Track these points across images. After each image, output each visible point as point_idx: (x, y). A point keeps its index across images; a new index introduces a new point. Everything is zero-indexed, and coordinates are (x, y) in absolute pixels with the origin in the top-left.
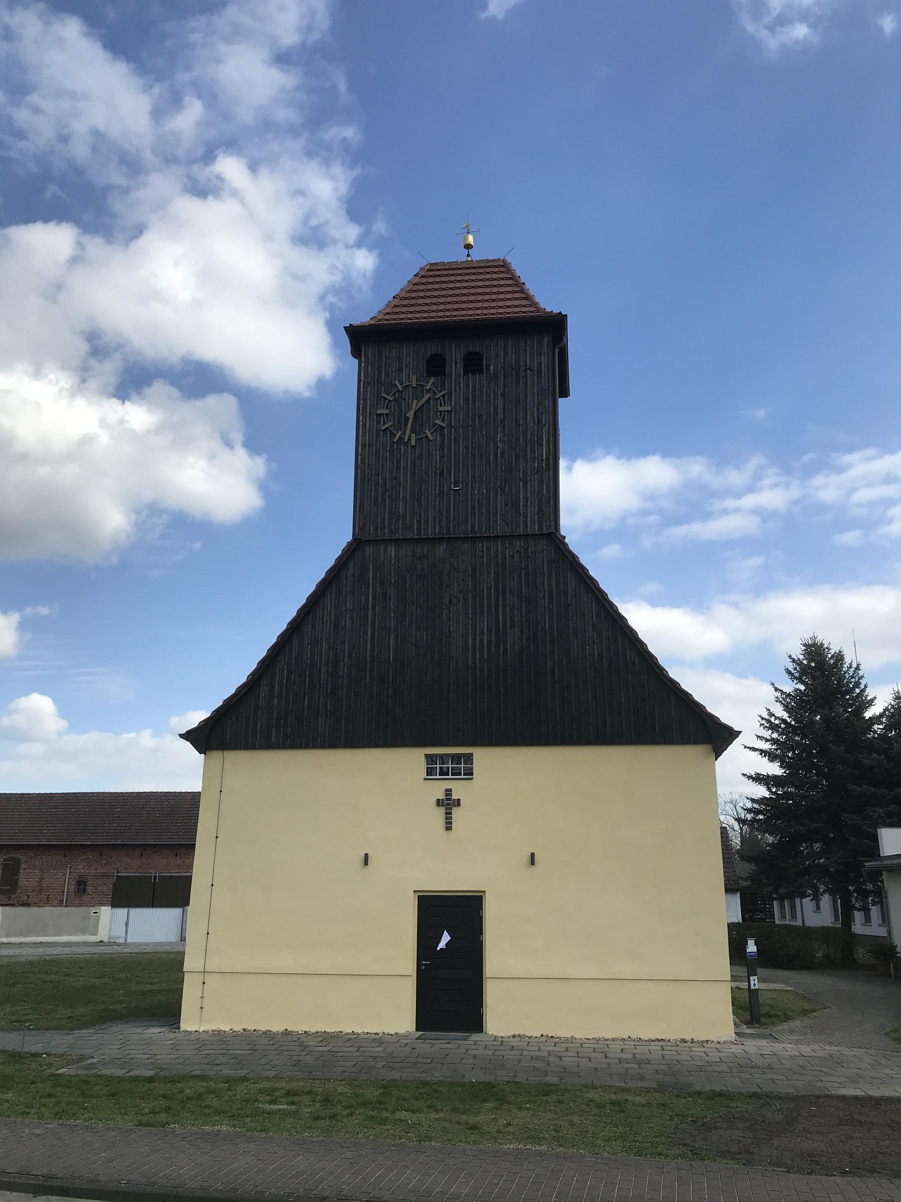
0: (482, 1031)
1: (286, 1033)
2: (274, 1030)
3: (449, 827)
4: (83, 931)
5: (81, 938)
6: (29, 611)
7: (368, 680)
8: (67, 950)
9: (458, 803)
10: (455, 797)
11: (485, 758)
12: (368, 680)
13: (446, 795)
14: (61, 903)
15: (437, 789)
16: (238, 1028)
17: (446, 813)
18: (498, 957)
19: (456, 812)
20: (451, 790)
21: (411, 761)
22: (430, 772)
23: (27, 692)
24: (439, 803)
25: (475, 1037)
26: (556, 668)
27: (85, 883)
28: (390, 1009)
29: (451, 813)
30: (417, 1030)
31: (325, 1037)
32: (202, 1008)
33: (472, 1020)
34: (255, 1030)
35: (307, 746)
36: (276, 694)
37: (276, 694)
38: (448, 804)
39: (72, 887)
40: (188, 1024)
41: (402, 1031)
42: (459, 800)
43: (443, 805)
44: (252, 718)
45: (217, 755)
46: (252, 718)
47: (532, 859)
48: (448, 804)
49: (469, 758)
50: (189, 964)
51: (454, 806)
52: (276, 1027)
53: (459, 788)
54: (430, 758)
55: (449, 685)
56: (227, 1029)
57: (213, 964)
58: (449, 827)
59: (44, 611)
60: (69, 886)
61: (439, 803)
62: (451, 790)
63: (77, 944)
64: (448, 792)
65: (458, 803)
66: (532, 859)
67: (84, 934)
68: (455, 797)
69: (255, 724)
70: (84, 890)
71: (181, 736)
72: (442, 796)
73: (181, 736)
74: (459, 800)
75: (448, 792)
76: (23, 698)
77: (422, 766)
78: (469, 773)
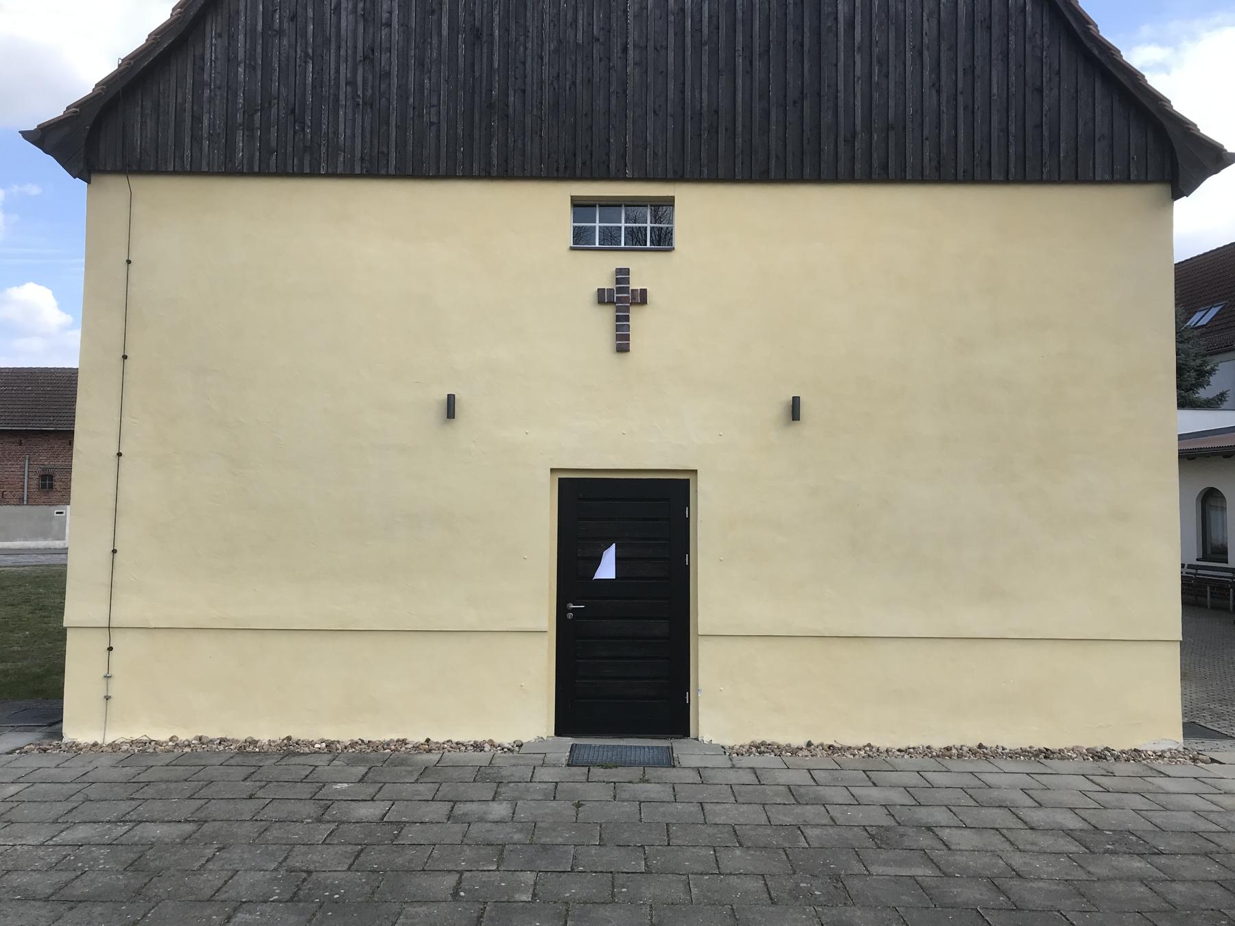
0: (686, 734)
1: (289, 749)
2: (264, 737)
3: (622, 344)
4: (45, 535)
5: (41, 544)
6: (16, 189)
7: (445, 32)
8: (32, 560)
9: (642, 298)
10: (635, 284)
11: (698, 208)
12: (445, 32)
13: (618, 281)
14: (20, 502)
15: (599, 269)
16: (184, 736)
17: (618, 319)
18: (724, 594)
19: (638, 317)
20: (627, 271)
21: (537, 212)
22: (581, 239)
23: (20, 282)
24: (603, 298)
25: (680, 747)
26: (858, 18)
27: (51, 477)
28: (507, 699)
29: (627, 318)
30: (560, 731)
31: (379, 763)
32: (107, 698)
33: (667, 711)
34: (222, 741)
35: (314, 173)
36: (241, 56)
37: (241, 56)
38: (622, 299)
39: (35, 482)
40: (79, 728)
41: (527, 737)
42: (644, 292)
43: (611, 302)
44: (188, 106)
45: (115, 188)
46: (188, 106)
47: (795, 410)
48: (622, 299)
49: (670, 202)
50: (79, 609)
51: (634, 303)
52: (267, 731)
53: (644, 269)
54: (580, 206)
55: (625, 50)
56: (162, 736)
57: (128, 610)
58: (622, 344)
59: (34, 190)
60: (30, 481)
61: (603, 298)
62: (627, 271)
63: (37, 551)
64: (622, 275)
65: (642, 298)
66: (795, 410)
67: (46, 539)
68: (635, 284)
69: (197, 119)
70: (51, 486)
71: (26, 135)
72: (608, 283)
73: (26, 135)
74: (644, 292)
75: (622, 275)
76: (15, 289)
77: (565, 223)
78: (663, 240)
